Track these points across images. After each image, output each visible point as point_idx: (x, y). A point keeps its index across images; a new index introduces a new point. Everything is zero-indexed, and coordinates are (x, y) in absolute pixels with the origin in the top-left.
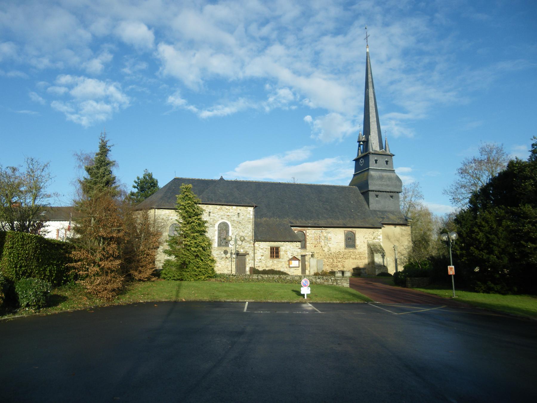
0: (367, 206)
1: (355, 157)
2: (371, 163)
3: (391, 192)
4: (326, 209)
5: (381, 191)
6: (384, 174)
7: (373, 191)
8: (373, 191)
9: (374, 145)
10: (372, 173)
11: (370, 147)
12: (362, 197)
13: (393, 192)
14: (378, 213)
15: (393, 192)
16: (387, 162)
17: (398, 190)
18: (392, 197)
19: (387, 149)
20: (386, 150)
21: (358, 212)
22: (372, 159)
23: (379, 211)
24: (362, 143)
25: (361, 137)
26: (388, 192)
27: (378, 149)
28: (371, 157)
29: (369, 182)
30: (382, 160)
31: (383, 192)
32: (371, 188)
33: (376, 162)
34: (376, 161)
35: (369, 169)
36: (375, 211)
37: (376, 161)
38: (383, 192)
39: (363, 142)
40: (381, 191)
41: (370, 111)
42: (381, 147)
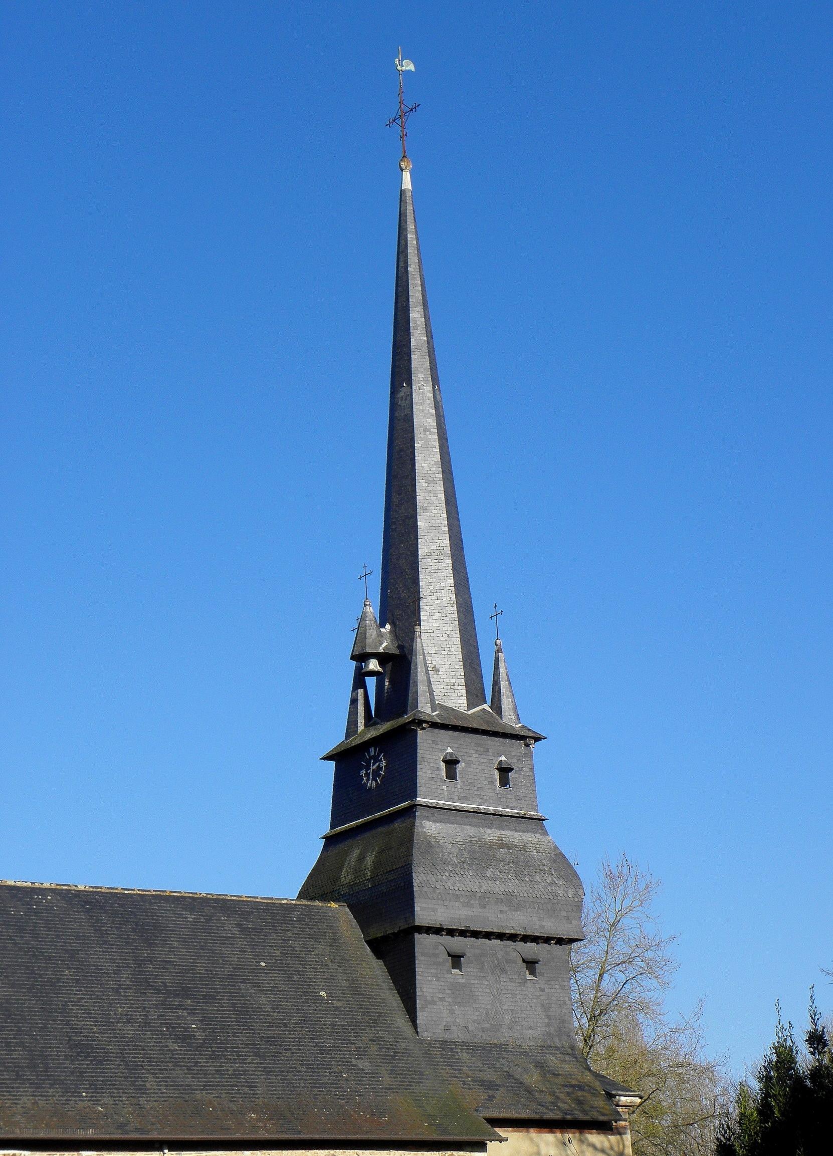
0: (401, 1021)
1: (336, 738)
2: (424, 773)
3: (526, 938)
4: (186, 1037)
5: (476, 934)
6: (492, 834)
7: (437, 931)
8: (437, 931)
9: (441, 680)
10: (428, 827)
11: (422, 688)
12: (374, 971)
13: (535, 939)
14: (463, 1055)
15: (535, 939)
16: (505, 771)
17: (563, 931)
18: (531, 964)
19: (506, 704)
20: (497, 706)
21: (362, 1053)
22: (431, 751)
23: (467, 1046)
24: (373, 665)
25: (372, 633)
26: (513, 937)
27: (458, 701)
28: (423, 737)
29: (418, 879)
30: (479, 759)
31: (488, 935)
32: (426, 911)
33: (451, 776)
34: (451, 763)
35: (410, 811)
36: (447, 1046)
37: (451, 763)
38: (488, 935)
39: (383, 658)
40: (476, 934)
41: (421, 497)
42: (475, 694)
